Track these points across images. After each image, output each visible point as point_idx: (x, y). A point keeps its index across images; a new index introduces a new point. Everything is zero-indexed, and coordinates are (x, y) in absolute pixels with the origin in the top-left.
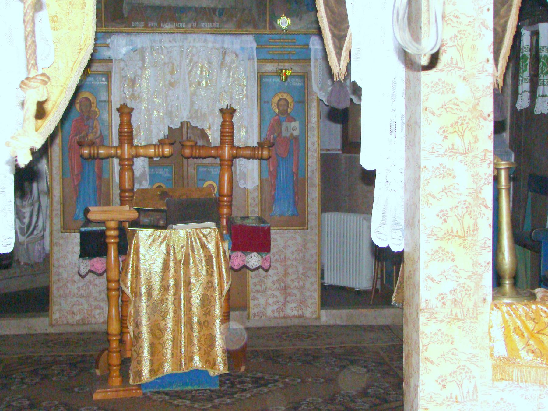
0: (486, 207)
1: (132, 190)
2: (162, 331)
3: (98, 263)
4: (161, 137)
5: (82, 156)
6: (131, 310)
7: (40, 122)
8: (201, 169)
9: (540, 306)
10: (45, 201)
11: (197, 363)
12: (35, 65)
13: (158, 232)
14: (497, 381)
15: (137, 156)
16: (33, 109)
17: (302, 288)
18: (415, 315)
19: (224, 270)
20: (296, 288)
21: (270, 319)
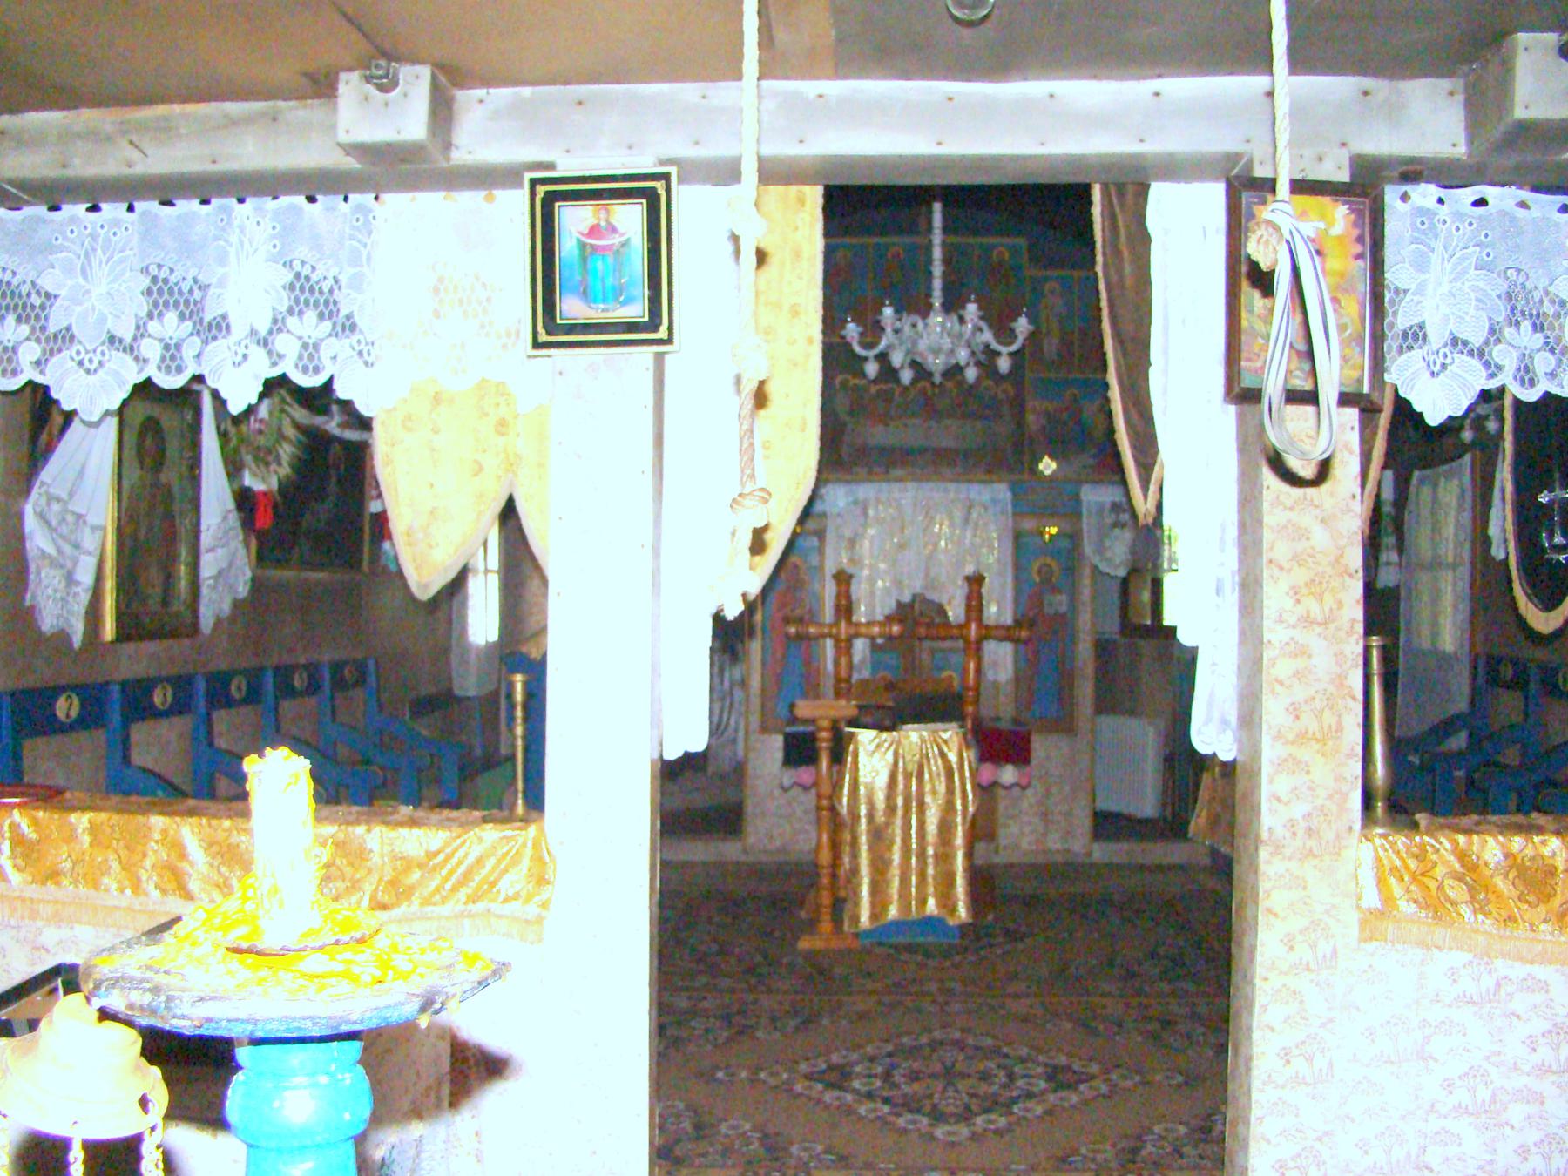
0: (1354, 698)
1: (848, 680)
2: (887, 863)
3: (805, 774)
4: (887, 611)
5: (787, 635)
6: (847, 837)
7: (757, 558)
8: (938, 656)
9: (1426, 838)
10: (739, 695)
11: (931, 906)
12: (752, 476)
13: (885, 735)
14: (1365, 941)
15: (857, 635)
16: (746, 539)
17: (1068, 814)
18: (1252, 848)
19: (969, 787)
20: (1060, 813)
21: (1025, 854)
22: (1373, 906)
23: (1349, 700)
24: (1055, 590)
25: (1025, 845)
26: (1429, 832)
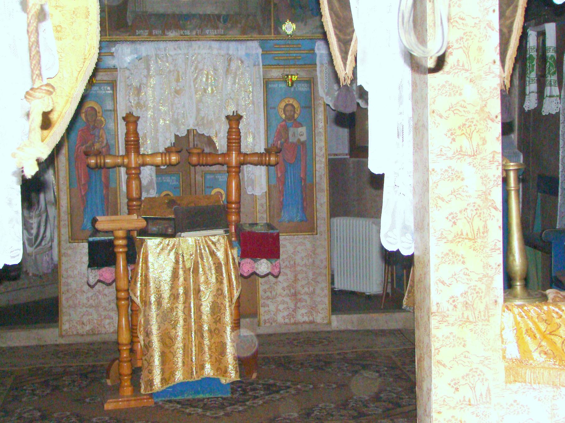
0: (496, 208)
1: (139, 199)
2: (172, 340)
3: (107, 273)
4: (168, 145)
5: (88, 166)
6: (141, 319)
7: (46, 132)
8: (209, 177)
9: (551, 307)
11: (209, 371)
12: (40, 75)
13: (167, 241)
15: (144, 165)
16: (38, 120)
18: (426, 318)
20: (306, 293)
21: (280, 325)
22: (514, 356)
23: (493, 210)
24: (299, 125)
25: (280, 319)
26: (555, 302)
